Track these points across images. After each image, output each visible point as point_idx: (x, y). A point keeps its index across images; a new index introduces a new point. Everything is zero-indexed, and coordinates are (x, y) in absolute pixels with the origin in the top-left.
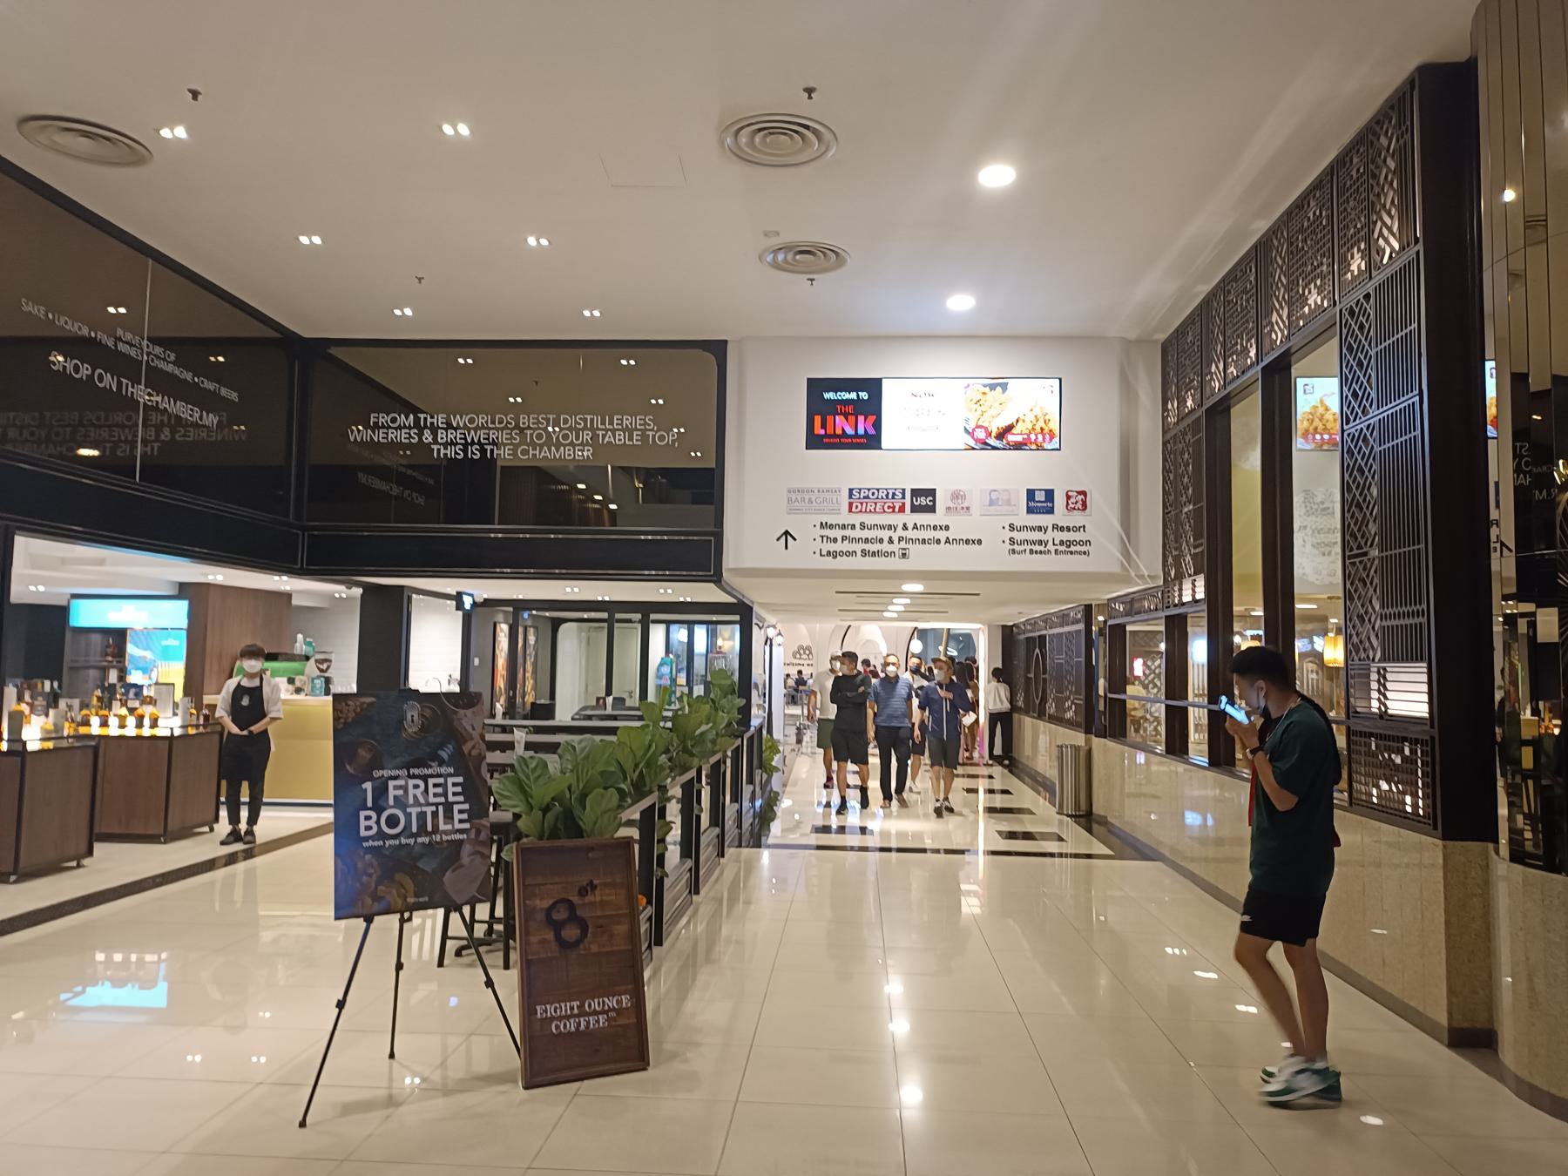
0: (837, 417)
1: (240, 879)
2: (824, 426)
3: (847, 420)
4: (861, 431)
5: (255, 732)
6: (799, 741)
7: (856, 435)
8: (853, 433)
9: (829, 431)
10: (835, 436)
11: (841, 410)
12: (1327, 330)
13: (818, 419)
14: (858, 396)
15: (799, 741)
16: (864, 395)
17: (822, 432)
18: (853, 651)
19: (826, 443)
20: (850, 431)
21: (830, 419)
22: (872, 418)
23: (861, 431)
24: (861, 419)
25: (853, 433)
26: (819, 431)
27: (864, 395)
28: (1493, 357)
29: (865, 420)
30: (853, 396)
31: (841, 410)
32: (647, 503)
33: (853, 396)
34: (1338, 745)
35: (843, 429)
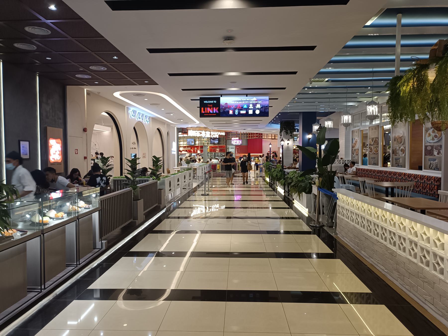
0: (208, 108)
1: (187, 172)
2: (204, 111)
3: (211, 109)
4: (214, 112)
5: (78, 184)
6: (341, 126)
7: (213, 113)
8: (212, 112)
9: (206, 112)
10: (207, 113)
11: (209, 106)
12: (226, 191)
13: (202, 109)
14: (213, 102)
15: (341, 126)
16: (215, 102)
17: (204, 112)
18: (76, 168)
19: (205, 115)
20: (211, 112)
21: (206, 108)
22: (217, 108)
23: (214, 112)
24: (214, 108)
25: (212, 112)
26: (203, 112)
27: (215, 102)
28: (373, 73)
29: (216, 109)
30: (212, 102)
31: (209, 106)
32: (370, 165)
33: (212, 102)
34: (389, 190)
35: (210, 112)
